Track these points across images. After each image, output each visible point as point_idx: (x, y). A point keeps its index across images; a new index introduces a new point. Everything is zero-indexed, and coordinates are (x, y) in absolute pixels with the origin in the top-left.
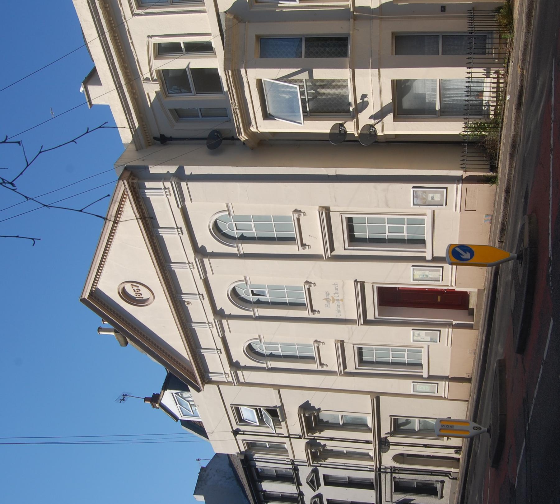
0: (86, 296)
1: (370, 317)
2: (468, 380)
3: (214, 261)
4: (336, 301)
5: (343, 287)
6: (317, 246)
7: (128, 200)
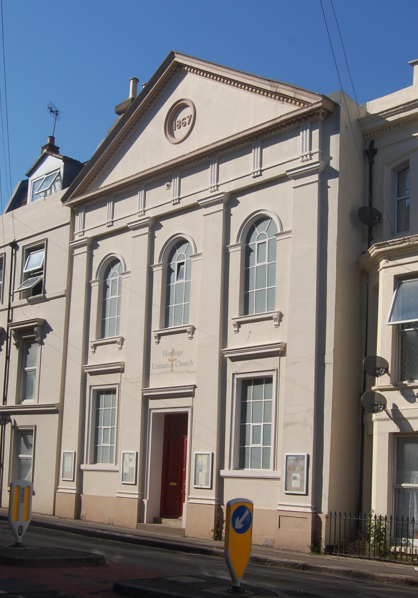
0: (178, 59)
1: (152, 404)
2: (78, 516)
6: (236, 342)
7: (297, 108)
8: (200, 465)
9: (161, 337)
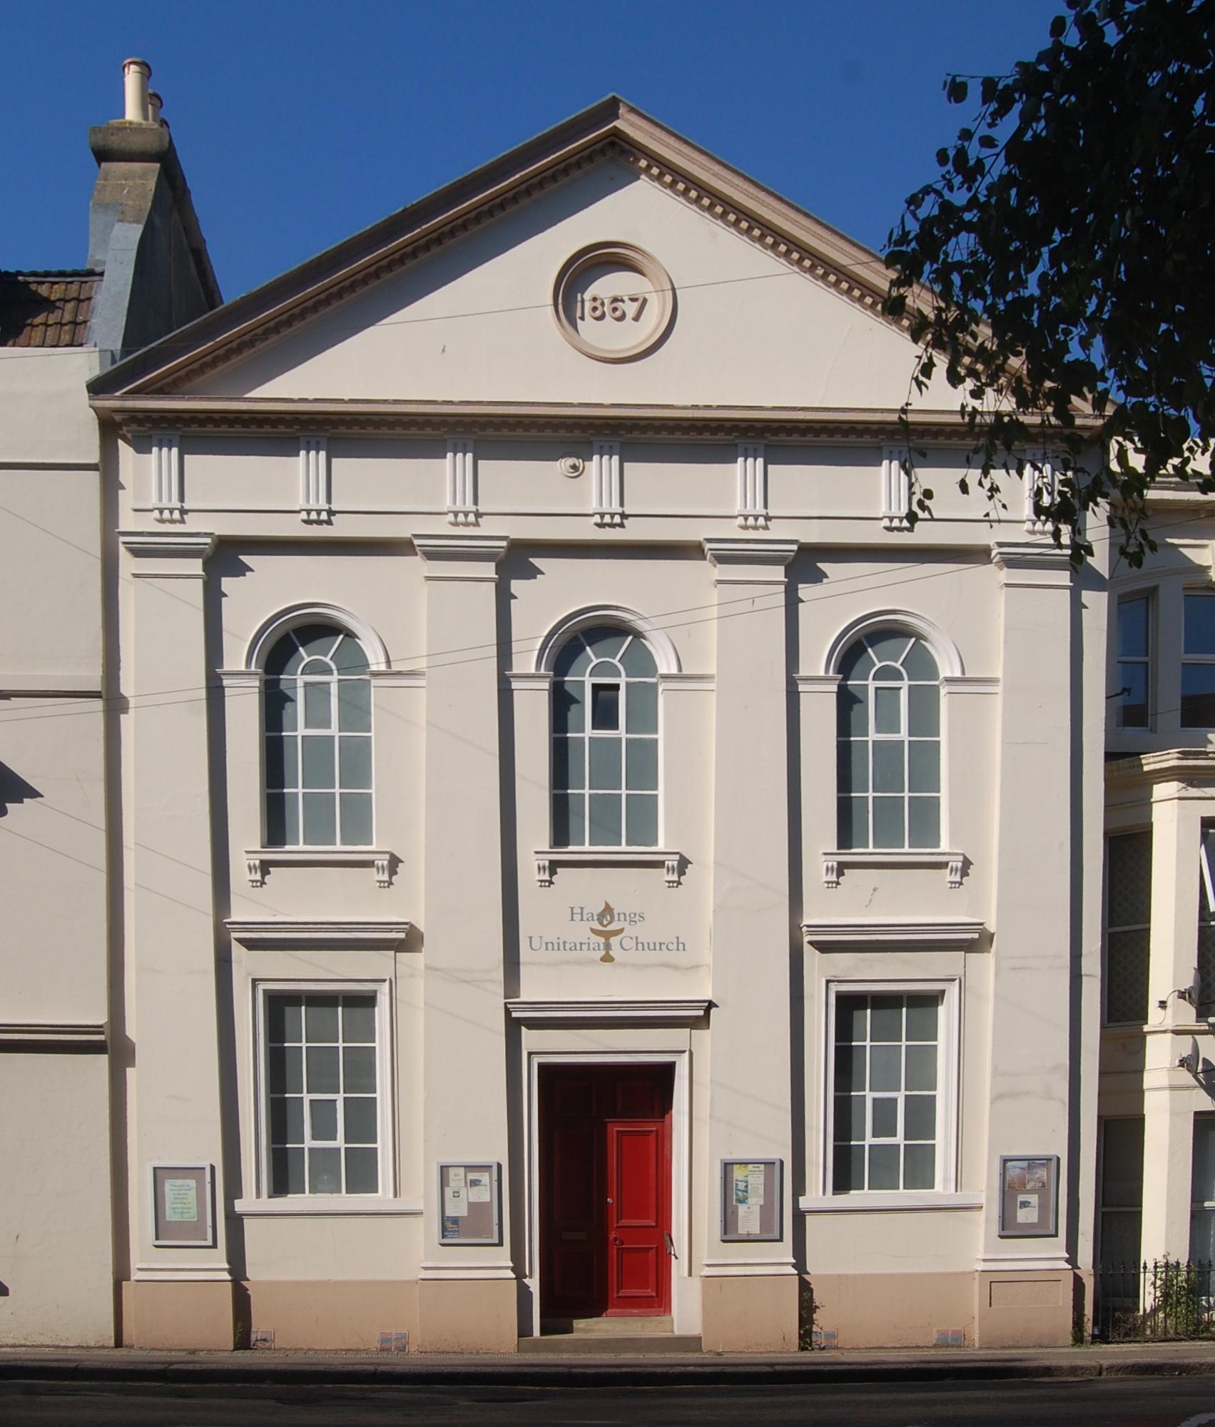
0: (627, 124)
1: (531, 1039)
2: (243, 1339)
3: (488, 592)
4: (602, 940)
6: (828, 908)
8: (741, 1186)
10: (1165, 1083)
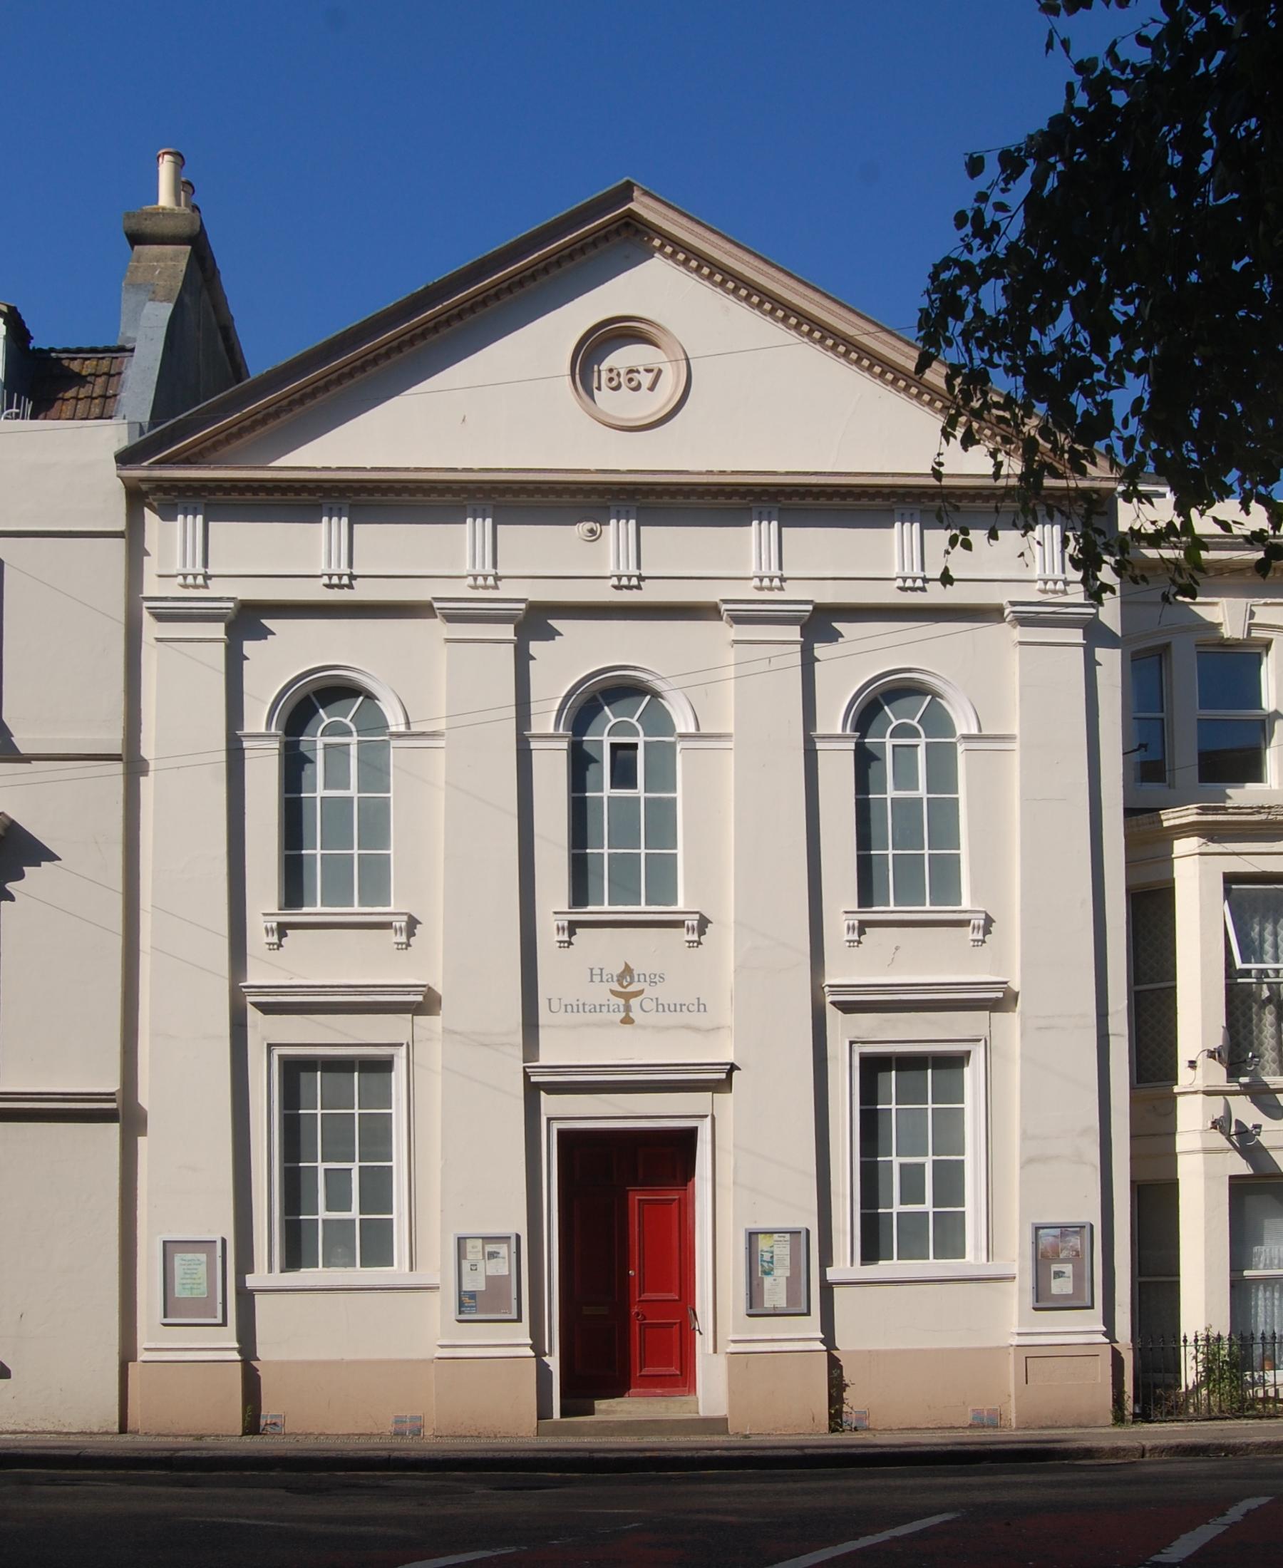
0: (642, 206)
1: (550, 1104)
2: (252, 1425)
4: (621, 1001)
5: (688, 1027)
6: (847, 968)
8: (767, 1257)
9: (578, 930)
10: (1198, 1145)
